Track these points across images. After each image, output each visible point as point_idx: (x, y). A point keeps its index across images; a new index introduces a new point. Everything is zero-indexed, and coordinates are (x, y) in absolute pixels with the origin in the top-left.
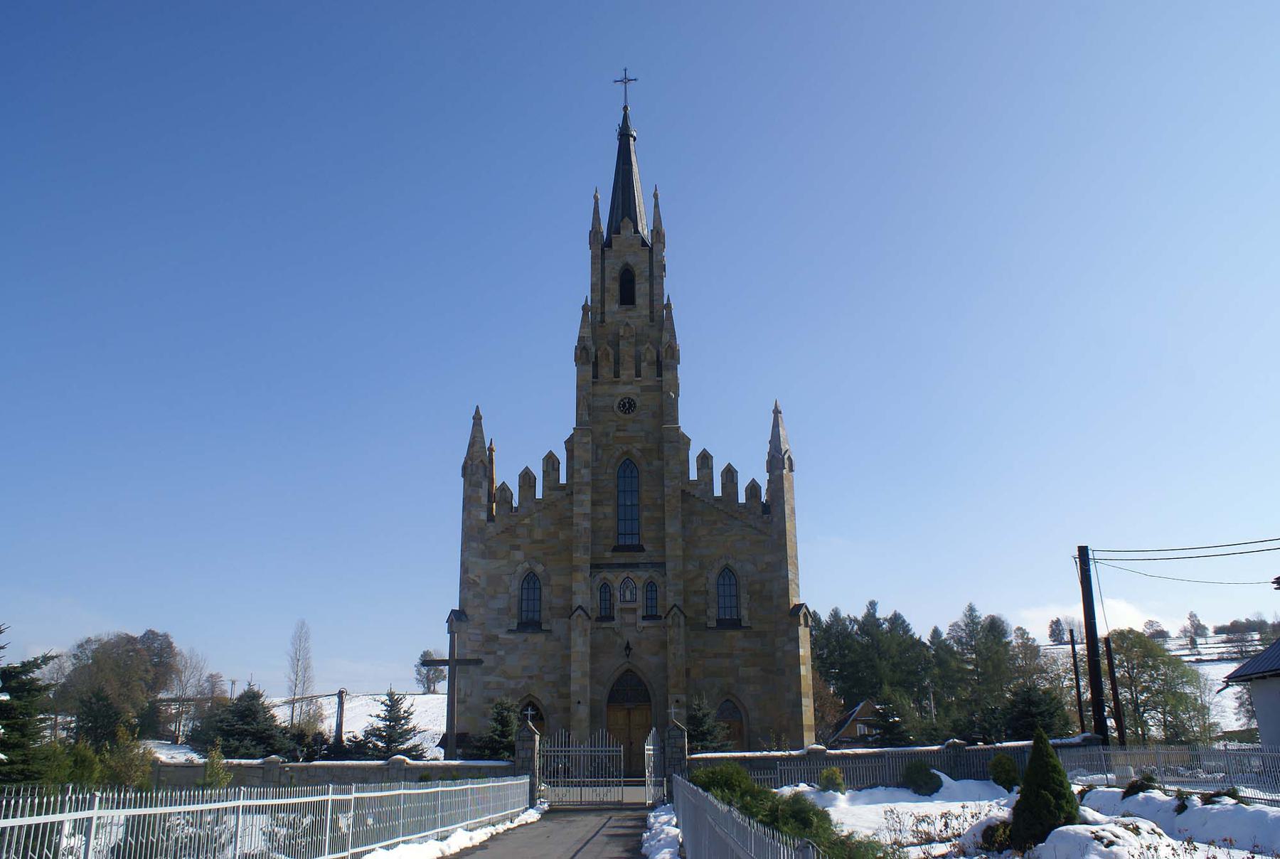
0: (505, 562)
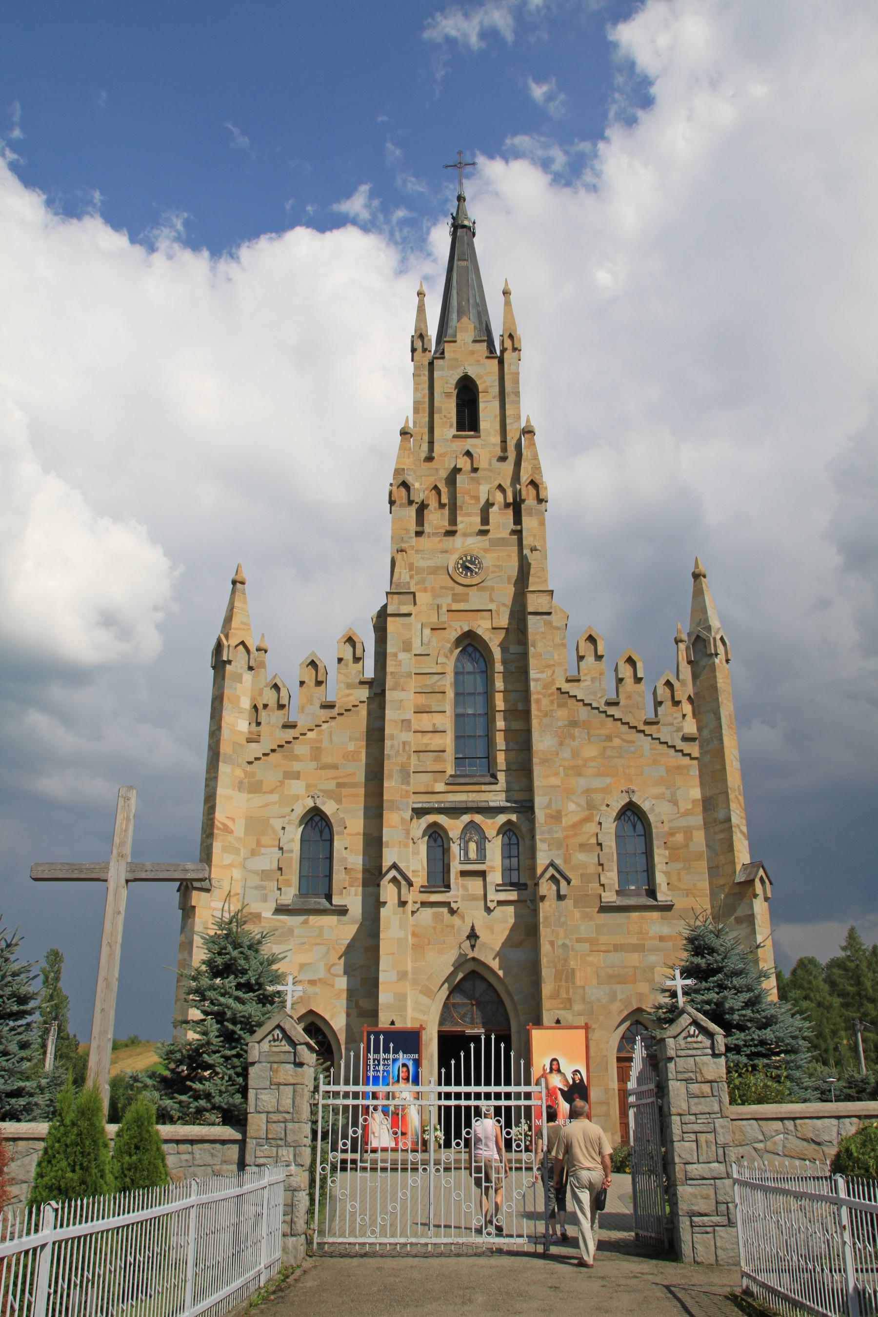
0: (275, 797)
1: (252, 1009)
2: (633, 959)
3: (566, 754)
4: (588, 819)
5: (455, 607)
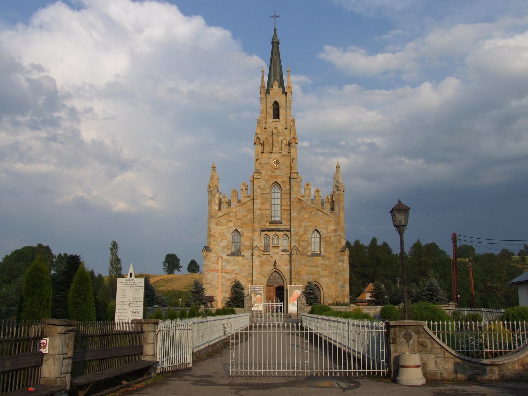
0: (225, 227)
1: (510, 316)
2: (315, 269)
3: (300, 216)
4: (305, 234)
5: (272, 175)
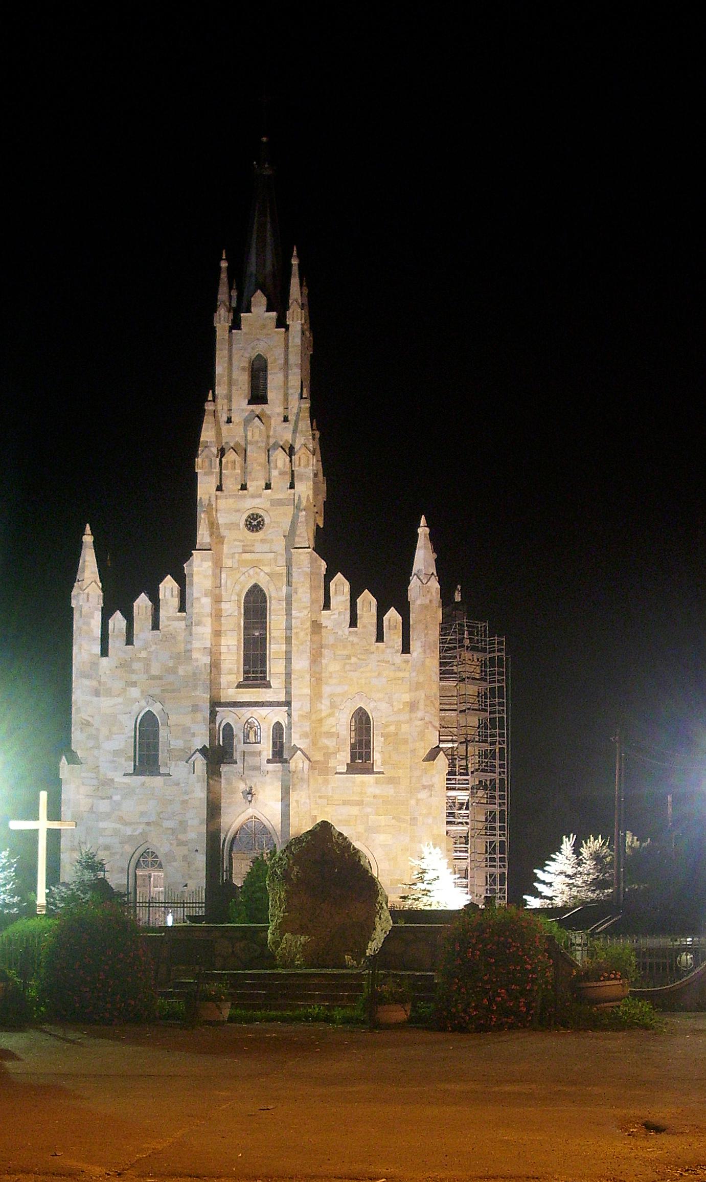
0: (120, 700)
2: (355, 810)
